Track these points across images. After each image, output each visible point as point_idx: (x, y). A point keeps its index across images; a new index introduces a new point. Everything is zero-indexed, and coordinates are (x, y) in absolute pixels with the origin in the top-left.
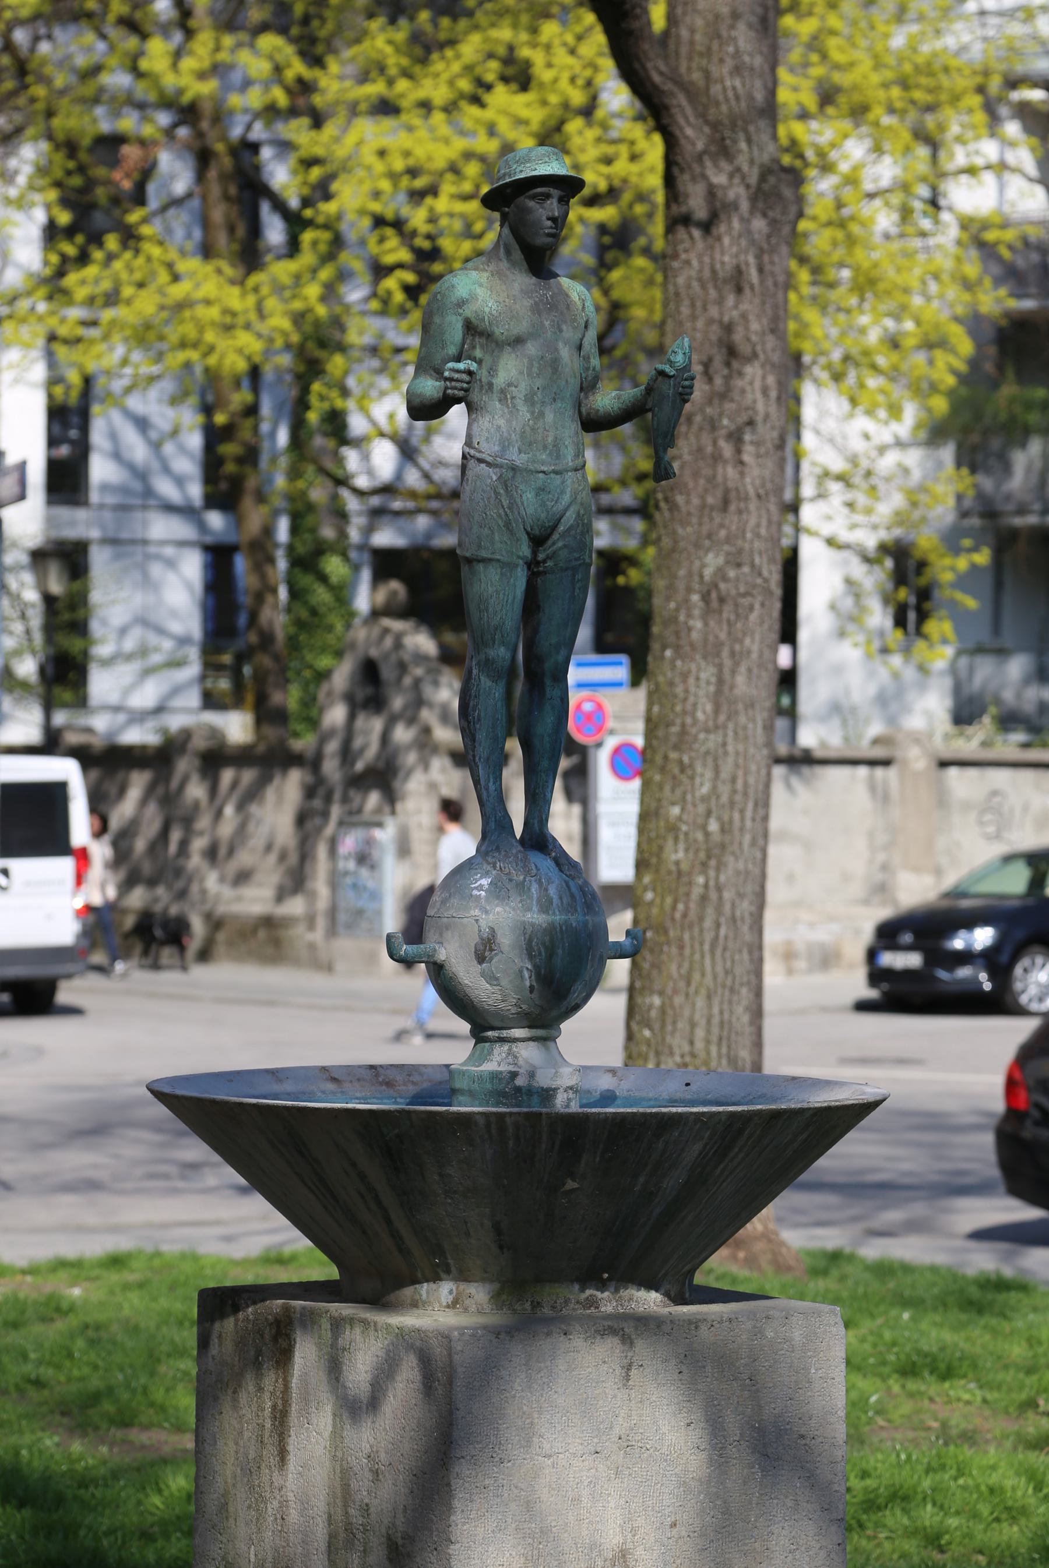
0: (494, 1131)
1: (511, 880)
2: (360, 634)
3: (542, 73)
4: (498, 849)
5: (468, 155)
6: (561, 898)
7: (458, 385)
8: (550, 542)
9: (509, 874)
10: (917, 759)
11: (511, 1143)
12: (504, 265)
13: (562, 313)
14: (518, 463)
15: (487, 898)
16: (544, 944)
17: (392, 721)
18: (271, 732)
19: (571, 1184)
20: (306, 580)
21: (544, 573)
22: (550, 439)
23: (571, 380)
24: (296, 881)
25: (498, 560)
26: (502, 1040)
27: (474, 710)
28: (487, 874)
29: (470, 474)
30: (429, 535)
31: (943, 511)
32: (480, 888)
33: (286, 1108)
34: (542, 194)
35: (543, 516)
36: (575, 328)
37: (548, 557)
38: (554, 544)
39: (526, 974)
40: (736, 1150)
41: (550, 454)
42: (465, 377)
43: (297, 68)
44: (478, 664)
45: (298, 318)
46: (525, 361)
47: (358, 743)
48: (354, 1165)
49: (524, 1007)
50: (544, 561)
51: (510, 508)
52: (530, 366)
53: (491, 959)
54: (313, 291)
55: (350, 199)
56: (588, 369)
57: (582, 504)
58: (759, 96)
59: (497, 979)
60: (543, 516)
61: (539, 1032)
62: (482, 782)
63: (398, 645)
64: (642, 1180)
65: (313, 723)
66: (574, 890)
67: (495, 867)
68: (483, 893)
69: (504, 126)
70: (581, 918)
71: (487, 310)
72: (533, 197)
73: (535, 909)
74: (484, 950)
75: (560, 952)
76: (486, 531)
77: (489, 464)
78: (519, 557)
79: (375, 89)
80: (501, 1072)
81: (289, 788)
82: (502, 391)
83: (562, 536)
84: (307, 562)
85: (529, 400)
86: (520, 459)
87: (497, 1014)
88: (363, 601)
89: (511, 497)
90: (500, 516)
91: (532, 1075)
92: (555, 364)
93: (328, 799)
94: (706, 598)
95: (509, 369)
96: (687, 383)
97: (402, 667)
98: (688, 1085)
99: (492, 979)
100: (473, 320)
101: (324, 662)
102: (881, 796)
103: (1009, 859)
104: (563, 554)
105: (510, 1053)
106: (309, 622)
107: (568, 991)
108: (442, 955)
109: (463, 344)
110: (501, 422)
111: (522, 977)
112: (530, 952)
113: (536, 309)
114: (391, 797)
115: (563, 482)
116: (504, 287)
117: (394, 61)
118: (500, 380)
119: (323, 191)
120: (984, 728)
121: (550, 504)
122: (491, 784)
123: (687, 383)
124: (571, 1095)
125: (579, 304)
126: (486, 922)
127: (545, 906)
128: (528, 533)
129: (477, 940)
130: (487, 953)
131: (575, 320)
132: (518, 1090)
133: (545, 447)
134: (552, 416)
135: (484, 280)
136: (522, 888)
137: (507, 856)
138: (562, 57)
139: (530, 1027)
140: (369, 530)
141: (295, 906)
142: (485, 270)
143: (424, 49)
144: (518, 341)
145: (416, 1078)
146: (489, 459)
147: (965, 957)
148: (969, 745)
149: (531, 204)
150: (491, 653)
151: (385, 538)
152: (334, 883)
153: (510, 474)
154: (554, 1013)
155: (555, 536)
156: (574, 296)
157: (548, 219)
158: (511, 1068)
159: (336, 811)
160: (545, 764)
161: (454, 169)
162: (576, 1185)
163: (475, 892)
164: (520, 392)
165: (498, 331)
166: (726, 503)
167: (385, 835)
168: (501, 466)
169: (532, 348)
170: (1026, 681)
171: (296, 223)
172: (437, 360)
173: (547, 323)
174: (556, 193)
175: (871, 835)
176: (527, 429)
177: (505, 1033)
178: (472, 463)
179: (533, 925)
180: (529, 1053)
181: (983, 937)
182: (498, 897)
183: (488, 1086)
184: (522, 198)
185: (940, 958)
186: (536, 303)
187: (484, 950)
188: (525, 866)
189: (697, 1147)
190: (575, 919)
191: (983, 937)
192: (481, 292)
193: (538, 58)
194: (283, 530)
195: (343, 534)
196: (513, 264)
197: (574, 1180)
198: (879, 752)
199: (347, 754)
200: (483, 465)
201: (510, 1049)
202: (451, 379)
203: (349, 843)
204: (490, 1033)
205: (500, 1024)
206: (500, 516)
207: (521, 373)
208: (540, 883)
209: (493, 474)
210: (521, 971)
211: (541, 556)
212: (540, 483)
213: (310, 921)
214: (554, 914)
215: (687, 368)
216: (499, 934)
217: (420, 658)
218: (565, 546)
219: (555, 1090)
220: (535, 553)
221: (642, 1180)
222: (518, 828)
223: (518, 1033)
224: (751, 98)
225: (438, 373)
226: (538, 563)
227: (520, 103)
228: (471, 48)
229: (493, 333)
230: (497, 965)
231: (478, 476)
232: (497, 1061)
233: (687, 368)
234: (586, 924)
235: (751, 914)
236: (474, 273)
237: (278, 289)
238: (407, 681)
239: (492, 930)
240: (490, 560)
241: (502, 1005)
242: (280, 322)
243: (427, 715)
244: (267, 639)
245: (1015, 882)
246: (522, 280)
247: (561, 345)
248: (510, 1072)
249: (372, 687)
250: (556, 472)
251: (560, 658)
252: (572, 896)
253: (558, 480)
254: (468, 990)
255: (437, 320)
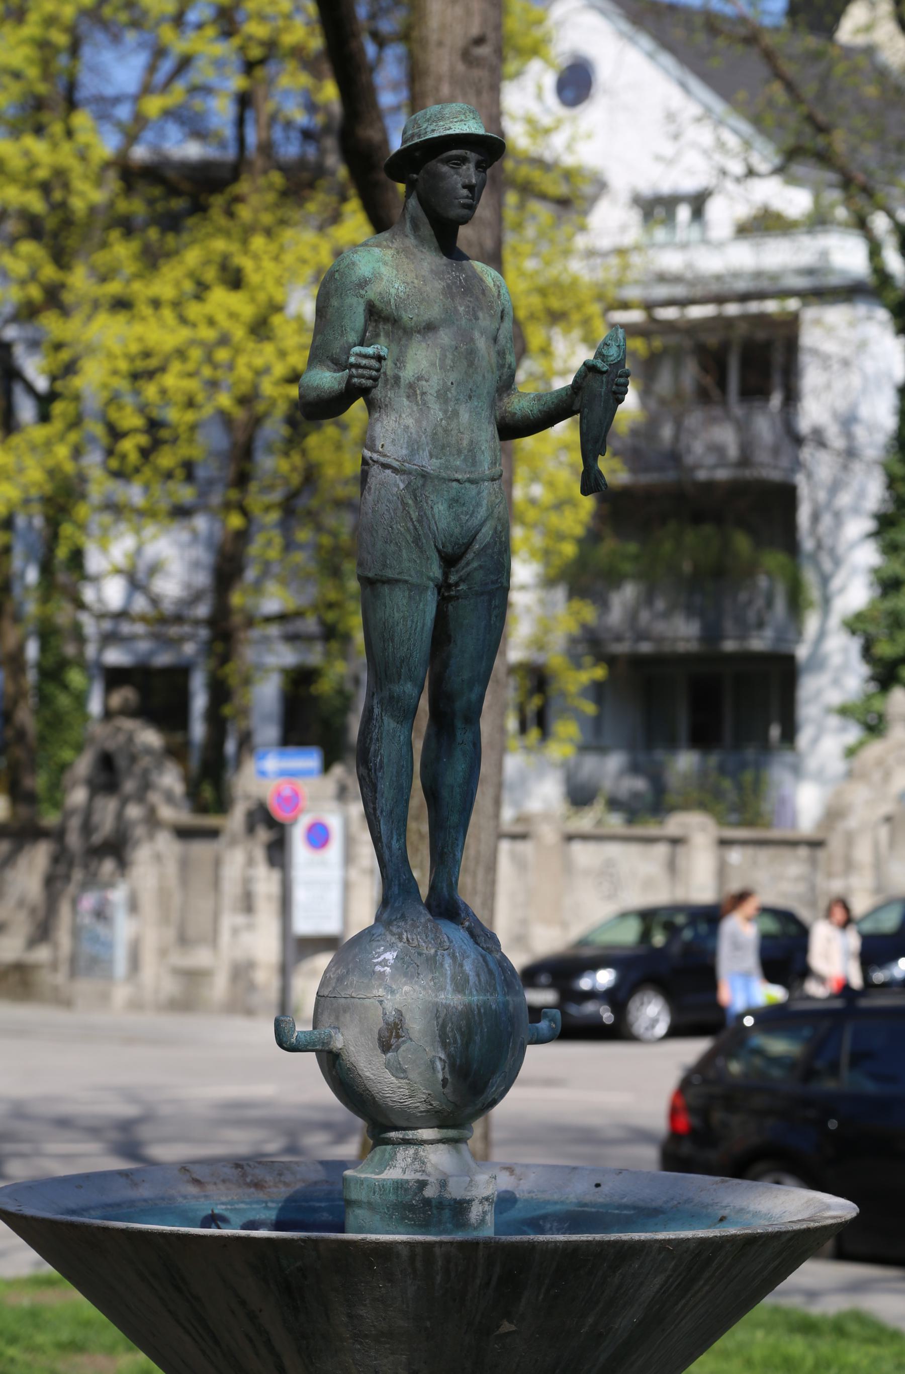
0: (419, 1265)
1: (420, 954)
2: (97, 729)
3: (252, 276)
4: (403, 917)
5: (193, 342)
6: (478, 975)
7: (366, 372)
8: (463, 562)
9: (419, 946)
10: (549, 834)
11: (439, 1279)
12: (411, 241)
13: (477, 299)
14: (429, 469)
15: (393, 976)
16: (459, 1029)
17: (124, 802)
18: (24, 811)
19: (507, 1327)
20: (51, 688)
21: (457, 598)
22: (465, 443)
23: (488, 376)
24: (43, 932)
25: (406, 582)
26: (407, 1142)
27: (376, 756)
28: (391, 947)
29: (373, 482)
30: (152, 653)
31: (558, 639)
32: (384, 963)
33: (162, 1235)
34: (457, 158)
35: (457, 531)
36: (492, 316)
37: (462, 580)
38: (468, 564)
39: (439, 1065)
40: (701, 1283)
41: (465, 460)
42: (373, 363)
43: (49, 272)
44: (381, 702)
45: (52, 473)
46: (438, 351)
47: (96, 818)
48: (243, 1303)
49: (435, 1103)
50: (457, 584)
51: (419, 521)
52: (443, 359)
53: (398, 1047)
54: (62, 452)
55: (92, 378)
56: (503, 366)
57: (499, 519)
58: (489, 244)
59: (404, 1071)
60: (457, 531)
61: (451, 1133)
62: (384, 839)
63: (130, 739)
64: (590, 1320)
65: (57, 804)
66: (492, 965)
67: (400, 939)
68: (388, 969)
69: (222, 319)
70: (501, 998)
71: (393, 291)
72: (447, 161)
73: (449, 988)
74: (390, 1037)
75: (477, 1038)
76: (392, 548)
77: (395, 470)
78: (429, 578)
79: (114, 288)
80: (407, 1181)
81: (39, 856)
82: (411, 386)
83: (478, 555)
84: (53, 672)
85: (442, 396)
86: (432, 465)
87: (404, 1113)
88: (95, 706)
89: (420, 509)
90: (408, 530)
91: (443, 1184)
92: (471, 355)
93: (71, 865)
95: (420, 360)
96: (622, 380)
97: (133, 759)
98: (598, 1185)
99: (398, 1070)
100: (377, 303)
101: (67, 754)
103: (624, 915)
104: (479, 576)
105: (416, 1157)
106: (54, 723)
107: (486, 1085)
108: (338, 1043)
109: (365, 331)
110: (410, 422)
111: (434, 1069)
112: (443, 1039)
113: (448, 291)
114: (123, 864)
115: (479, 493)
116: (412, 266)
117: (130, 267)
118: (408, 373)
119: (70, 369)
120: (597, 810)
121: (464, 518)
122: (394, 842)
123: (622, 380)
124: (487, 1207)
125: (494, 289)
126: (391, 1003)
127: (461, 986)
128: (439, 551)
129: (381, 1024)
130: (393, 1041)
131: (491, 308)
132: (427, 1202)
133: (459, 452)
134: (467, 416)
135: (388, 258)
136: (433, 963)
137: (414, 926)
138: (268, 264)
139: (440, 1127)
140: (101, 650)
141: (42, 954)
142: (389, 247)
143: (152, 260)
144: (430, 328)
145: (288, 1178)
146: (396, 464)
147: (591, 995)
148: (586, 821)
149: (445, 169)
150: (397, 689)
151: (114, 657)
152: (76, 932)
153: (420, 482)
154: (469, 1110)
155: (470, 556)
156: (489, 282)
157: (464, 187)
158: (419, 1176)
159: (78, 875)
160: (454, 819)
161: (181, 354)
162: (513, 1328)
163: (378, 968)
164: (432, 386)
165: (406, 316)
167: (118, 895)
168: (409, 473)
169: (445, 337)
170: (622, 773)
171: (45, 403)
172: (336, 348)
173: (461, 309)
174: (473, 156)
176: (440, 430)
177: (410, 1134)
178: (375, 470)
179: (447, 1007)
180: (439, 1158)
181: (605, 978)
182: (405, 975)
183: (392, 1197)
184: (434, 162)
185: (570, 997)
186: (448, 286)
187: (390, 1037)
188: (436, 938)
189: (659, 1280)
190: (495, 1000)
191: (605, 978)
192: (385, 271)
193: (247, 264)
194: (32, 650)
195: (81, 653)
196: (421, 240)
197: (511, 1322)
198: (518, 829)
199: (87, 828)
200: (388, 472)
201: (416, 1153)
202: (358, 366)
203: (88, 901)
204: (393, 1135)
205: (404, 1124)
206: (408, 530)
207: (433, 364)
208: (454, 957)
209: (399, 482)
210: (433, 1062)
211: (453, 579)
212: (453, 493)
213: (54, 966)
214: (471, 993)
215: (620, 364)
216: (407, 1017)
217: (148, 751)
218: (481, 567)
219: (469, 1202)
220: (446, 575)
221: (590, 1320)
222: (424, 891)
223: (426, 1134)
224: (481, 246)
225: (339, 364)
226: (449, 587)
227: (236, 301)
228: (192, 257)
229: (400, 318)
230: (405, 1053)
231: (382, 484)
232: (399, 1168)
233: (620, 364)
234: (506, 1004)
236: (377, 250)
237: (33, 448)
238: (137, 769)
239: (399, 1012)
240: (397, 581)
241: (409, 1102)
242: (35, 474)
243: (154, 797)
244: (21, 735)
245: (628, 934)
246: (430, 261)
247: (477, 335)
248: (418, 1181)
249: (108, 774)
250: (471, 481)
251: (474, 696)
252: (490, 972)
253: (473, 490)
254: (369, 1084)
255: (335, 302)
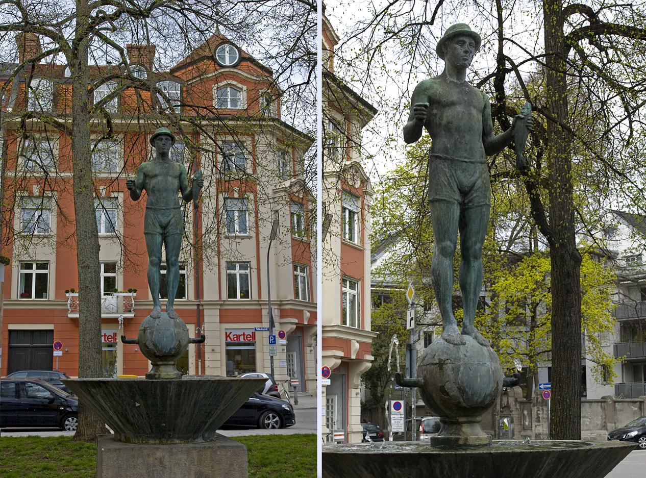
21: (468, 209)
25: (445, 200)
50: (468, 203)
72: (457, 43)
94: (564, 348)
102: (604, 409)
133: (466, 151)
166: (568, 325)
175: (602, 416)
235: (458, 439)
